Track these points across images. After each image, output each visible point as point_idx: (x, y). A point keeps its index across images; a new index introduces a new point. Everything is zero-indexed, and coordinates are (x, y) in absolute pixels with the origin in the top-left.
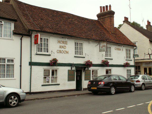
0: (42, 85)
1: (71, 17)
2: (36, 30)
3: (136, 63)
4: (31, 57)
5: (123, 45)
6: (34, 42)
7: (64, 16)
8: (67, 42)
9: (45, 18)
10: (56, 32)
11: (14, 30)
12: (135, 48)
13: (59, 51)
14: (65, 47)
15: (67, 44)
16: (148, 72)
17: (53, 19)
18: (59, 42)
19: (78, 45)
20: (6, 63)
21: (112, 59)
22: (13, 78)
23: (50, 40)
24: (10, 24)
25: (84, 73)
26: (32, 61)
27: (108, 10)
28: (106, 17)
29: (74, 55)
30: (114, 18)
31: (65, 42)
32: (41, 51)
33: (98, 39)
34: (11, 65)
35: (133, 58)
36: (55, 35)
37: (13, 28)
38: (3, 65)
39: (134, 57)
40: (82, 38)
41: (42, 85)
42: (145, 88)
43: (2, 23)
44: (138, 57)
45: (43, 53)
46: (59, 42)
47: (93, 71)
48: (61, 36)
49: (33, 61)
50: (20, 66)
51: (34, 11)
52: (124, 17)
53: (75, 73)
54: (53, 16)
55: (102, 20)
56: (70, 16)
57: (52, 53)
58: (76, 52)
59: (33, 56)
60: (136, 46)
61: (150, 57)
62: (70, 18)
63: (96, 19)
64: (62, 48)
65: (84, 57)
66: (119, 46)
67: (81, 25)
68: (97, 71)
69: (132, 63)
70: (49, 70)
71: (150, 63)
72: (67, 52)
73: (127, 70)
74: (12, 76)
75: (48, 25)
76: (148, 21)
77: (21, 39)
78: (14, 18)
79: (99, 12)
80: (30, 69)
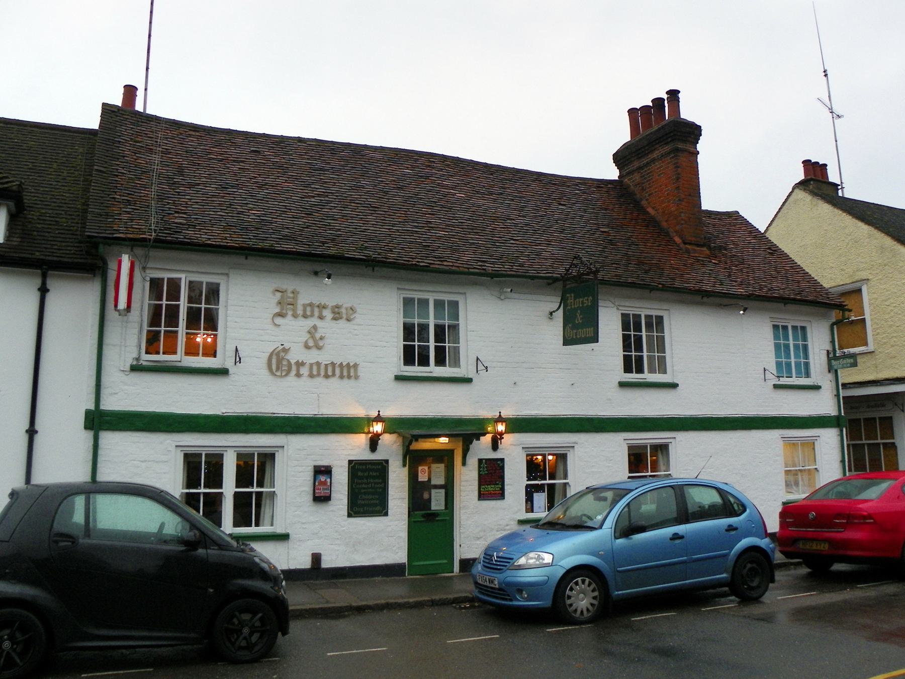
3: (850, 403)
5: (741, 303)
19: (786, 338)
21: (674, 386)
23: (227, 289)
26: (102, 407)
28: (653, 160)
30: (700, 158)
32: (640, 370)
35: (830, 376)
40: (465, 273)
48: (309, 266)
49: (110, 404)
52: (804, 162)
57: (767, 372)
59: (114, 375)
63: (612, 173)
65: (469, 381)
77: (44, 291)
79: (622, 135)
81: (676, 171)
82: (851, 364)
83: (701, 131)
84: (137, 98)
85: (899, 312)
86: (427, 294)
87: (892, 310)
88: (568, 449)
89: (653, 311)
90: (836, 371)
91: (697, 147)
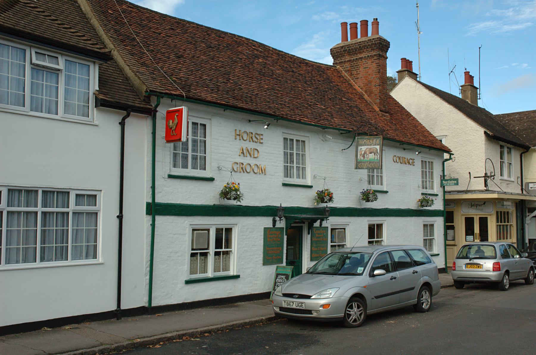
0: (188, 282)
1: (261, 52)
2: (171, 94)
4: (153, 187)
5: (417, 148)
6: (164, 135)
7: (240, 49)
8: (261, 137)
9: (188, 52)
10: (232, 102)
11: (98, 89)
12: (446, 156)
13: (238, 166)
14: (256, 152)
15: (262, 141)
16: (477, 230)
17: (213, 59)
18: (239, 136)
19: (292, 149)
20: (72, 206)
22: (91, 261)
24: (85, 70)
25: (309, 236)
26: (157, 201)
27: (370, 34)
29: (280, 178)
31: (257, 136)
33: (349, 128)
34: (89, 214)
36: (228, 112)
37: (95, 86)
38: (63, 213)
39: (443, 186)
41: (188, 282)
42: (509, 281)
43: (58, 65)
44: (457, 184)
45: (190, 172)
46: (238, 137)
47: (332, 229)
49: (160, 199)
50: (118, 217)
51: (150, 28)
52: (402, 59)
53: (285, 237)
54: (211, 47)
55: (347, 65)
56: (257, 50)
58: (286, 168)
60: (448, 151)
61: (486, 185)
62: (257, 57)
63: (329, 61)
64: (248, 155)
66: (404, 149)
67: (294, 82)
68: (344, 229)
69: (438, 205)
70: (208, 230)
71: (484, 204)
72: (263, 171)
73: (424, 225)
74: (91, 252)
75: (201, 78)
76: (467, 73)
77: (122, 124)
78: (98, 46)
80: (150, 228)
81: (378, 68)
82: (455, 183)
83: (389, 45)
84: (486, 109)
85: (463, 155)
86: (205, 120)
87: (459, 154)
88: (346, 226)
89: (198, 119)
90: (444, 187)
91: (387, 55)
